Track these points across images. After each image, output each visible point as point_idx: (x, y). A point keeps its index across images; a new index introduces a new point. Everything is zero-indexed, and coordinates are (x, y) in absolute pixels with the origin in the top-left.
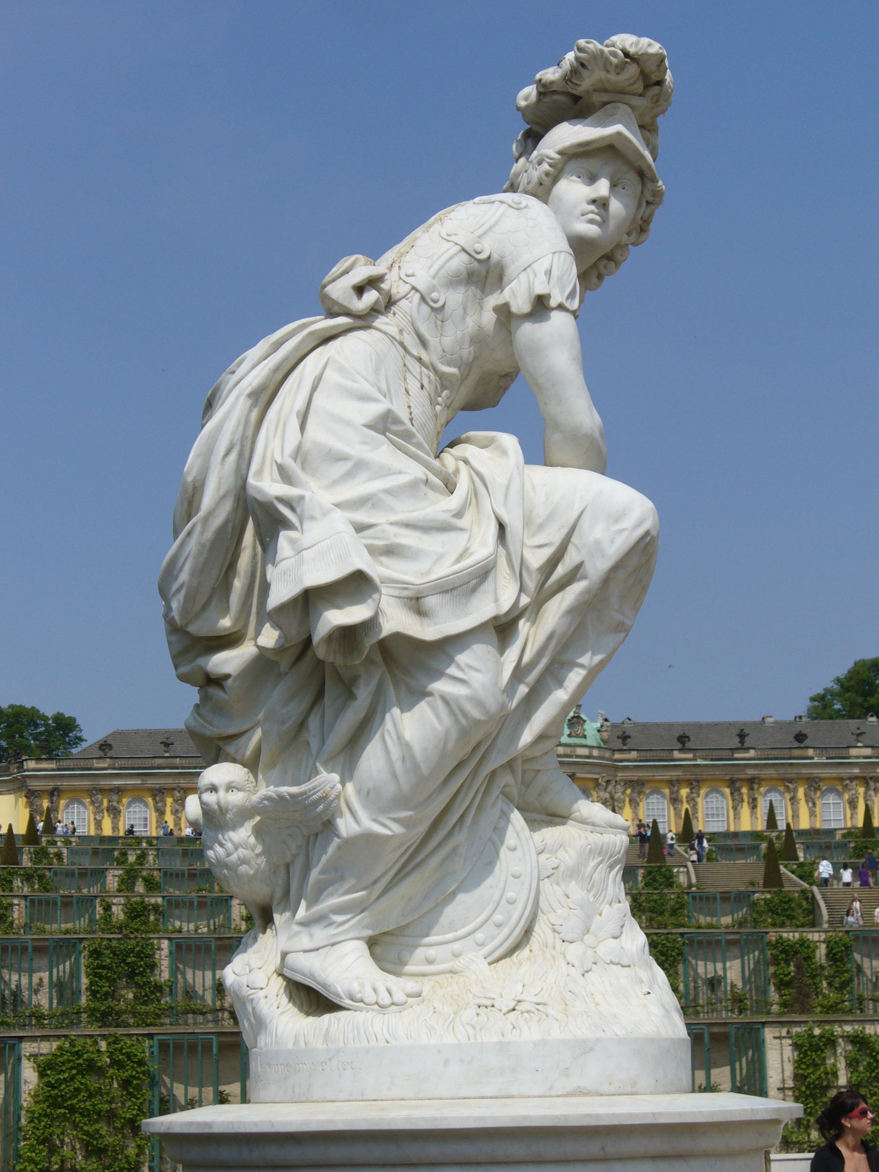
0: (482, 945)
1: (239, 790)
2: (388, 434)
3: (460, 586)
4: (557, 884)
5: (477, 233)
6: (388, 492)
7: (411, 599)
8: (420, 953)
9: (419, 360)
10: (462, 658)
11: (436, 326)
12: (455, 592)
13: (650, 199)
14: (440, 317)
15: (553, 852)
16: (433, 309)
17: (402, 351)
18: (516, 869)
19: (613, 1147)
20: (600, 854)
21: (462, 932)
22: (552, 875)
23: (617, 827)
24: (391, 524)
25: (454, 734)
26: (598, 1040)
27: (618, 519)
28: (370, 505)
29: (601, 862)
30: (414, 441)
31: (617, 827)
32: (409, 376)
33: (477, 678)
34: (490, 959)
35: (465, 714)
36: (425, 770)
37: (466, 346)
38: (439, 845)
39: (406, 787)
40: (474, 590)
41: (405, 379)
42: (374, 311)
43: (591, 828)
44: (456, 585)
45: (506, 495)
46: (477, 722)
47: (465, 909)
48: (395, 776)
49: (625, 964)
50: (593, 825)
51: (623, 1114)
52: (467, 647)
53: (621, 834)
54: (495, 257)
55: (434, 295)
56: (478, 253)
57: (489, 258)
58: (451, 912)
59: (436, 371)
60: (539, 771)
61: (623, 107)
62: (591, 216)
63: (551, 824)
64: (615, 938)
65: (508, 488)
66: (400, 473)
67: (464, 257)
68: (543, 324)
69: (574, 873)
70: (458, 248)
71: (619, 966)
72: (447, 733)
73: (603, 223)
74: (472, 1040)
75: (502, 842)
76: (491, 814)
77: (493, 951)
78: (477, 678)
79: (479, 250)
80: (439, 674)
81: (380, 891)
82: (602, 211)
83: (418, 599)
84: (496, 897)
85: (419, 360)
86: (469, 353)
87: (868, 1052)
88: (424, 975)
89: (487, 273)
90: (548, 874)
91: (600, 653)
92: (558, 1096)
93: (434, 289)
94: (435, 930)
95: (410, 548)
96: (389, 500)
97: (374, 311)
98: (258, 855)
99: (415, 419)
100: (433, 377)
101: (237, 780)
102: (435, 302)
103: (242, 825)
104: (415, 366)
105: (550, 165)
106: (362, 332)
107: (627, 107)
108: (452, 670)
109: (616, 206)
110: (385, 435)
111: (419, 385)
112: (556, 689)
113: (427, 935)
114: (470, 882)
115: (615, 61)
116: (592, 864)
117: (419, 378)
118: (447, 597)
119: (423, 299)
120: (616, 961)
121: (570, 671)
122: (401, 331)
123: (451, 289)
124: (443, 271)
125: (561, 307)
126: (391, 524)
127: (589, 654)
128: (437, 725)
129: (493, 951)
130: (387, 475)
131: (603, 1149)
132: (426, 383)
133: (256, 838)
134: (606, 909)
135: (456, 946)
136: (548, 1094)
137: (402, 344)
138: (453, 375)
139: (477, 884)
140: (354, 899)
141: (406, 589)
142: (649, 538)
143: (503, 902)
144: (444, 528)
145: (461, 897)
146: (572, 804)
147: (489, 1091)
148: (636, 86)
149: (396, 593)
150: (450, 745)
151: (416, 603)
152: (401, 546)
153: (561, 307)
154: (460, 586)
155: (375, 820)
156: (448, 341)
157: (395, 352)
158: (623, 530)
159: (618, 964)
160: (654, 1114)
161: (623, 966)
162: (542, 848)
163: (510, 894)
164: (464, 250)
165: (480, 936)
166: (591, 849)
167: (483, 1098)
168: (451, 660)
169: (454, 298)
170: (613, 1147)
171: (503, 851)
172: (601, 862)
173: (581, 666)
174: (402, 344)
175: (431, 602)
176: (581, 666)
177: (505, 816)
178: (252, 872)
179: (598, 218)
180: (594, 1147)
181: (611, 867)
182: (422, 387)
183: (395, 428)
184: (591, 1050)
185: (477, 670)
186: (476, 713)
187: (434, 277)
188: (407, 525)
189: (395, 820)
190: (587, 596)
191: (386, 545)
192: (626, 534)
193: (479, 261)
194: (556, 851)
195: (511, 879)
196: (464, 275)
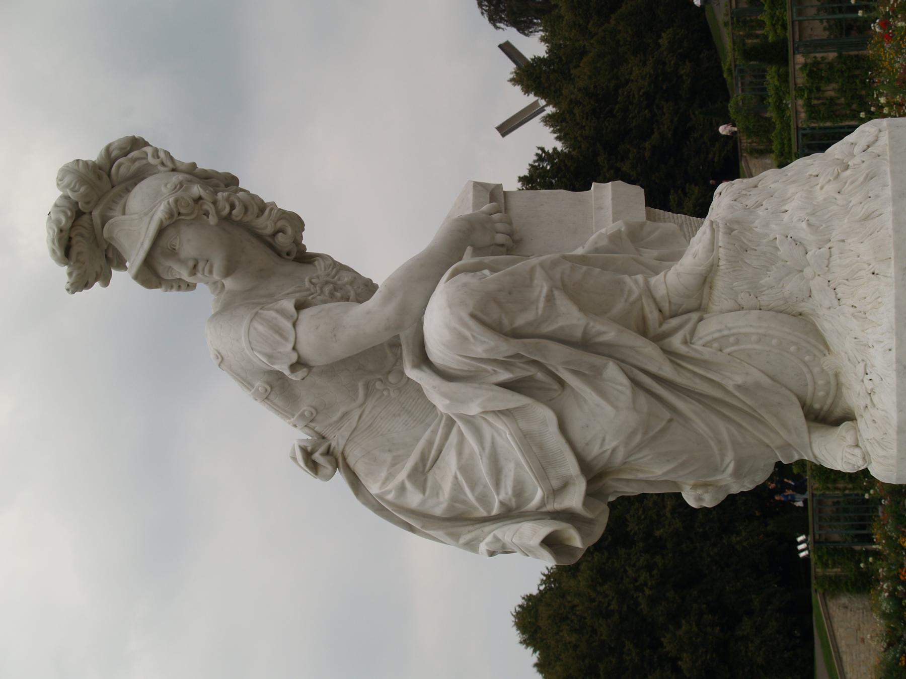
6: (472, 489)
21: (805, 370)
56: (266, 390)
60: (670, 302)
61: (106, 234)
67: (272, 397)
77: (820, 350)
95: (514, 487)
129: (820, 350)
135: (816, 370)
155: (723, 471)
175: (556, 483)
188: (497, 484)
192: (475, 334)
193: (272, 388)
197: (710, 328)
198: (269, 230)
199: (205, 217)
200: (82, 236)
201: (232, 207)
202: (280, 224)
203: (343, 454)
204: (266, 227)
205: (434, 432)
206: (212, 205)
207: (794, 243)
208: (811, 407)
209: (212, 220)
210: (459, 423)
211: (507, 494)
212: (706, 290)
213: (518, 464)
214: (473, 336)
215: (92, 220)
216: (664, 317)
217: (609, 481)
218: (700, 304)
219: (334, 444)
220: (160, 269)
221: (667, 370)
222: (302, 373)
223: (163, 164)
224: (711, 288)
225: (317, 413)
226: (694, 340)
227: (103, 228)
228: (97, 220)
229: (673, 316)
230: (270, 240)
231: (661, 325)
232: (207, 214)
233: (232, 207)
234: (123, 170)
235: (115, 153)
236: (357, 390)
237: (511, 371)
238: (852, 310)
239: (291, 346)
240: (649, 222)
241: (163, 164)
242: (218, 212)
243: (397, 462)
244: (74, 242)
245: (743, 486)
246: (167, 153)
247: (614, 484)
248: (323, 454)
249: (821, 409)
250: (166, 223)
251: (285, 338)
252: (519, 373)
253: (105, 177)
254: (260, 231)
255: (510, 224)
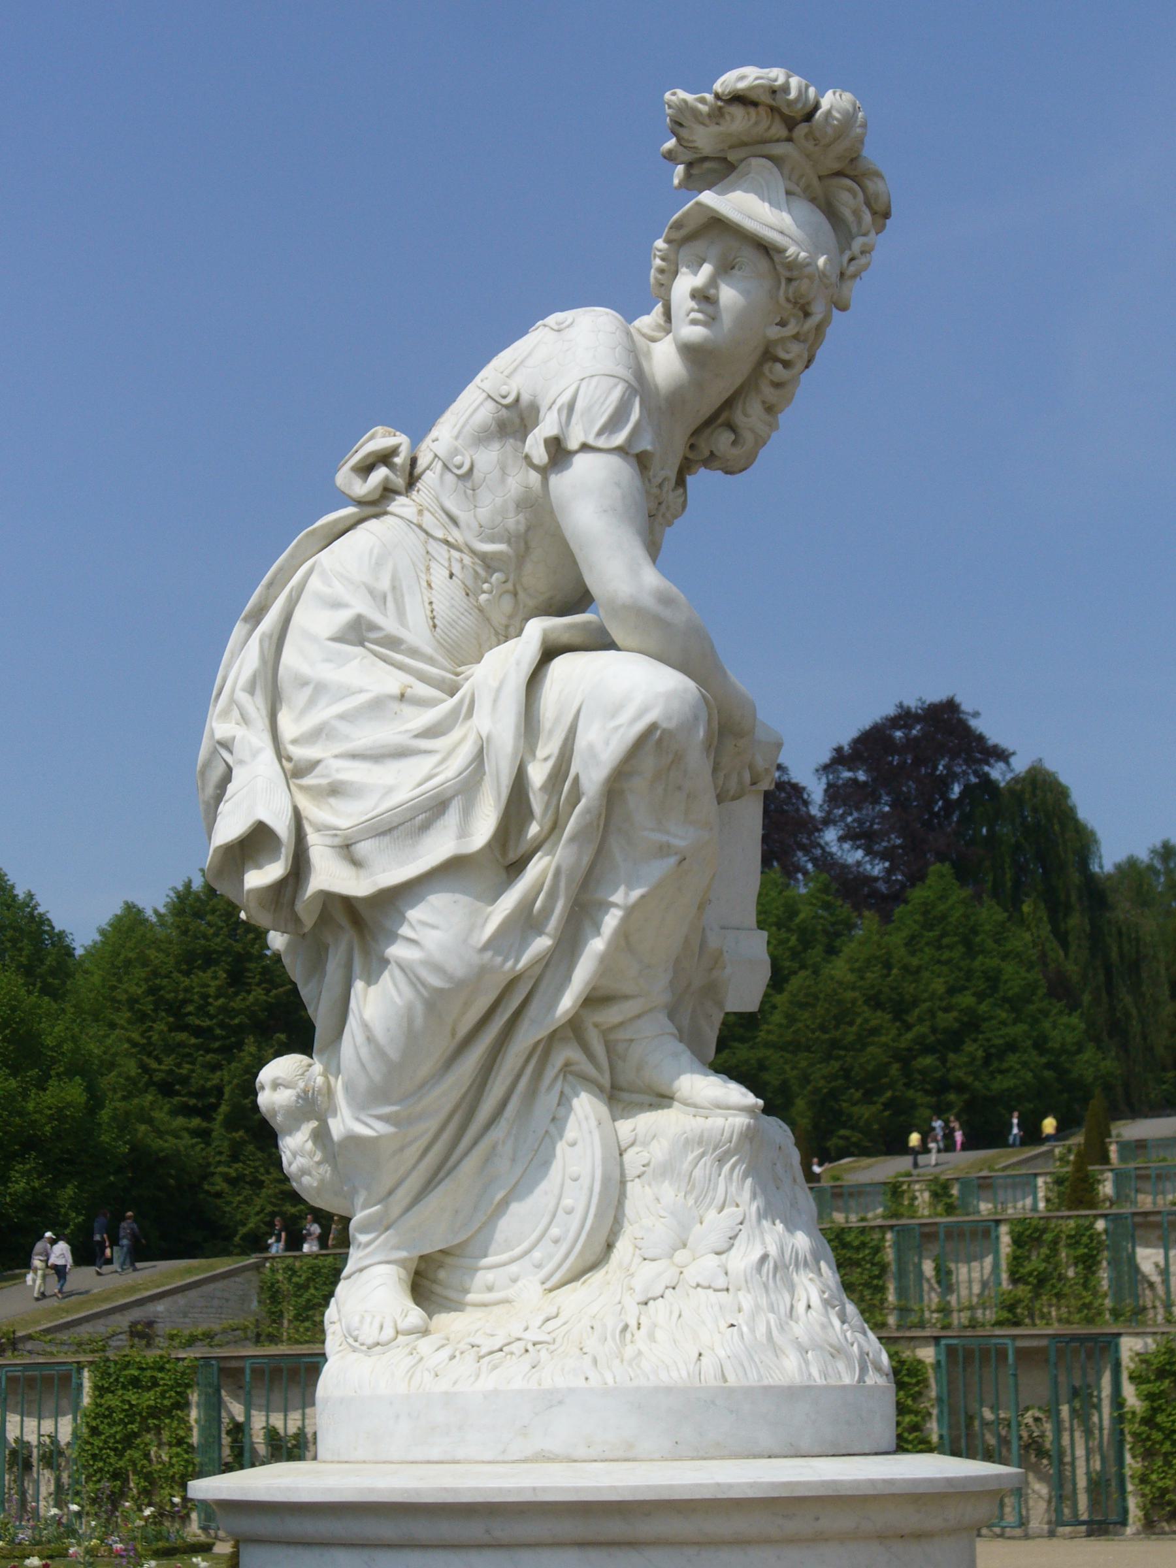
0: (539, 1266)
1: (287, 1087)
2: (367, 644)
3: (400, 825)
4: (650, 1185)
5: (506, 373)
6: (342, 717)
7: (341, 847)
8: (483, 1278)
9: (447, 542)
10: (413, 914)
11: (467, 497)
12: (395, 833)
13: (788, 274)
14: (469, 485)
15: (645, 1144)
16: (458, 477)
17: (422, 535)
18: (574, 1169)
19: (502, 1530)
20: (700, 1143)
21: (518, 1251)
22: (643, 1173)
23: (728, 1108)
24: (336, 756)
25: (419, 1008)
26: (571, 1391)
27: (613, 715)
28: (324, 736)
29: (703, 1155)
30: (403, 647)
31: (728, 1108)
32: (433, 565)
33: (440, 935)
34: (548, 1285)
35: (423, 984)
36: (393, 1054)
37: (511, 514)
38: (475, 1143)
39: (377, 1078)
40: (425, 827)
41: (428, 569)
42: (387, 492)
43: (692, 1110)
44: (395, 824)
45: (495, 701)
46: (440, 991)
47: (519, 1221)
48: (363, 1065)
49: (719, 1287)
50: (695, 1106)
51: (491, 1489)
52: (421, 899)
53: (735, 1115)
54: (526, 398)
55: (458, 459)
56: (504, 397)
57: (517, 400)
58: (506, 1226)
59: (473, 552)
60: (632, 1040)
61: (755, 162)
62: (693, 315)
63: (652, 1107)
64: (718, 1253)
65: (499, 690)
66: (361, 691)
67: (490, 405)
68: (565, 473)
69: (666, 1170)
70: (484, 395)
71: (710, 1291)
72: (410, 1008)
73: (712, 320)
74: (593, 1382)
75: (561, 1136)
76: (547, 1100)
77: (552, 1275)
78: (440, 935)
79: (504, 393)
80: (393, 937)
81: (408, 1200)
82: (705, 306)
83: (348, 846)
84: (551, 1207)
85: (447, 542)
86: (518, 523)
87: (118, 1437)
88: (485, 1305)
89: (522, 419)
90: (638, 1173)
91: (640, 887)
92: (513, 1462)
93: (456, 452)
94: (492, 1249)
95: (352, 783)
96: (343, 727)
97: (387, 492)
98: (319, 1163)
99: (438, 617)
100: (467, 560)
101: (282, 1075)
102: (459, 467)
103: (298, 1129)
104: (440, 551)
105: (663, 259)
106: (374, 521)
107: (763, 161)
108: (405, 930)
109: (728, 295)
110: (364, 646)
111: (447, 574)
112: (593, 938)
113: (485, 1256)
114: (519, 1190)
115: (704, 108)
116: (691, 1157)
117: (446, 565)
118: (386, 839)
119: (446, 467)
120: (705, 1284)
121: (606, 913)
122: (420, 512)
123: (482, 448)
124: (465, 430)
125: (585, 447)
126: (336, 756)
127: (622, 889)
128: (398, 1000)
129: (552, 1275)
130: (347, 696)
131: (487, 1531)
132: (456, 569)
133: (315, 1143)
134: (711, 1215)
135: (514, 1268)
136: (500, 1458)
137: (420, 527)
138: (501, 553)
139: (530, 1190)
140: (370, 1215)
141: (336, 835)
142: (658, 733)
143: (560, 1212)
144: (401, 753)
145: (515, 1208)
146: (673, 1080)
147: (435, 1454)
148: (773, 131)
149: (329, 841)
150: (419, 1021)
151: (347, 850)
152: (342, 783)
153: (585, 447)
154: (400, 825)
155: (358, 1119)
156: (484, 513)
157: (414, 539)
158: (620, 726)
159: (709, 1287)
160: (534, 1489)
161: (715, 1290)
162: (632, 1139)
163: (567, 1202)
164: (489, 396)
165: (537, 1255)
166: (687, 1138)
167: (429, 1462)
168: (402, 919)
169: (487, 458)
170: (502, 1530)
171: (561, 1147)
172: (703, 1155)
173: (616, 905)
174: (420, 527)
175: (364, 848)
176: (616, 905)
177: (564, 1101)
178: (315, 1184)
179: (699, 316)
180: (475, 1530)
181: (721, 1161)
182: (451, 576)
183: (373, 635)
184: (560, 1402)
185: (434, 927)
186: (435, 981)
187: (457, 438)
188: (354, 756)
189: (379, 1118)
190: (588, 817)
191: (329, 784)
192: (622, 730)
193: (507, 407)
194: (649, 1144)
195: (568, 1182)
196: (494, 427)
197: (586, 1108)
198: (739, 418)
199: (778, 320)
200: (756, 123)
201: (787, 364)
202: (749, 437)
203: (386, 513)
204: (746, 415)
205: (431, 661)
206: (794, 332)
207: (732, 1234)
208: (441, 1266)
209: (774, 332)
210: (452, 702)
211: (338, 770)
212: (647, 1099)
213: (389, 791)
214: (617, 728)
215: (778, 141)
216: (606, 1033)
217: (348, 935)
218: (621, 1089)
219: (401, 500)
220: (699, 246)
221: (528, 1036)
222: (540, 455)
223: (852, 259)
224: (651, 1105)
225: (458, 477)
226: (570, 1077)
227: (764, 157)
228: (780, 149)
229: (609, 1048)
230: (720, 421)
231: (596, 1025)
232: (782, 324)
233: (787, 364)
234: (845, 196)
235: (871, 185)
236: (493, 542)
237: (544, 788)
238: (633, 1324)
239: (591, 441)
240: (718, 1018)
241: (852, 259)
242: (782, 340)
243: (380, 599)
244: (752, 110)
245: (294, 1155)
246: (866, 267)
247: (343, 947)
248: (387, 479)
249: (434, 1281)
250: (776, 258)
251: (600, 433)
252: (537, 803)
253: (836, 166)
254: (740, 405)
255: (734, 798)
